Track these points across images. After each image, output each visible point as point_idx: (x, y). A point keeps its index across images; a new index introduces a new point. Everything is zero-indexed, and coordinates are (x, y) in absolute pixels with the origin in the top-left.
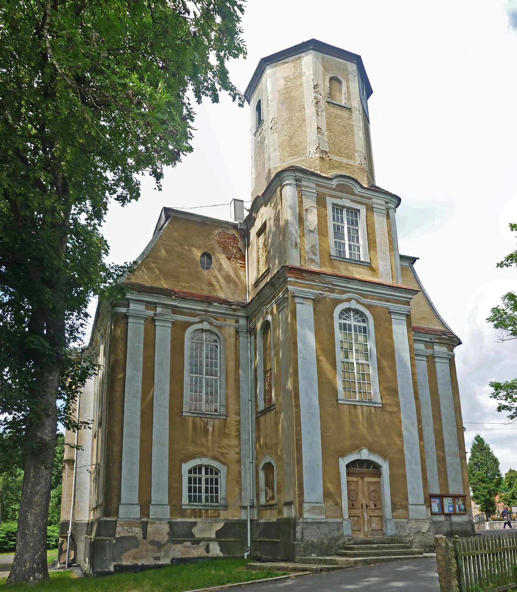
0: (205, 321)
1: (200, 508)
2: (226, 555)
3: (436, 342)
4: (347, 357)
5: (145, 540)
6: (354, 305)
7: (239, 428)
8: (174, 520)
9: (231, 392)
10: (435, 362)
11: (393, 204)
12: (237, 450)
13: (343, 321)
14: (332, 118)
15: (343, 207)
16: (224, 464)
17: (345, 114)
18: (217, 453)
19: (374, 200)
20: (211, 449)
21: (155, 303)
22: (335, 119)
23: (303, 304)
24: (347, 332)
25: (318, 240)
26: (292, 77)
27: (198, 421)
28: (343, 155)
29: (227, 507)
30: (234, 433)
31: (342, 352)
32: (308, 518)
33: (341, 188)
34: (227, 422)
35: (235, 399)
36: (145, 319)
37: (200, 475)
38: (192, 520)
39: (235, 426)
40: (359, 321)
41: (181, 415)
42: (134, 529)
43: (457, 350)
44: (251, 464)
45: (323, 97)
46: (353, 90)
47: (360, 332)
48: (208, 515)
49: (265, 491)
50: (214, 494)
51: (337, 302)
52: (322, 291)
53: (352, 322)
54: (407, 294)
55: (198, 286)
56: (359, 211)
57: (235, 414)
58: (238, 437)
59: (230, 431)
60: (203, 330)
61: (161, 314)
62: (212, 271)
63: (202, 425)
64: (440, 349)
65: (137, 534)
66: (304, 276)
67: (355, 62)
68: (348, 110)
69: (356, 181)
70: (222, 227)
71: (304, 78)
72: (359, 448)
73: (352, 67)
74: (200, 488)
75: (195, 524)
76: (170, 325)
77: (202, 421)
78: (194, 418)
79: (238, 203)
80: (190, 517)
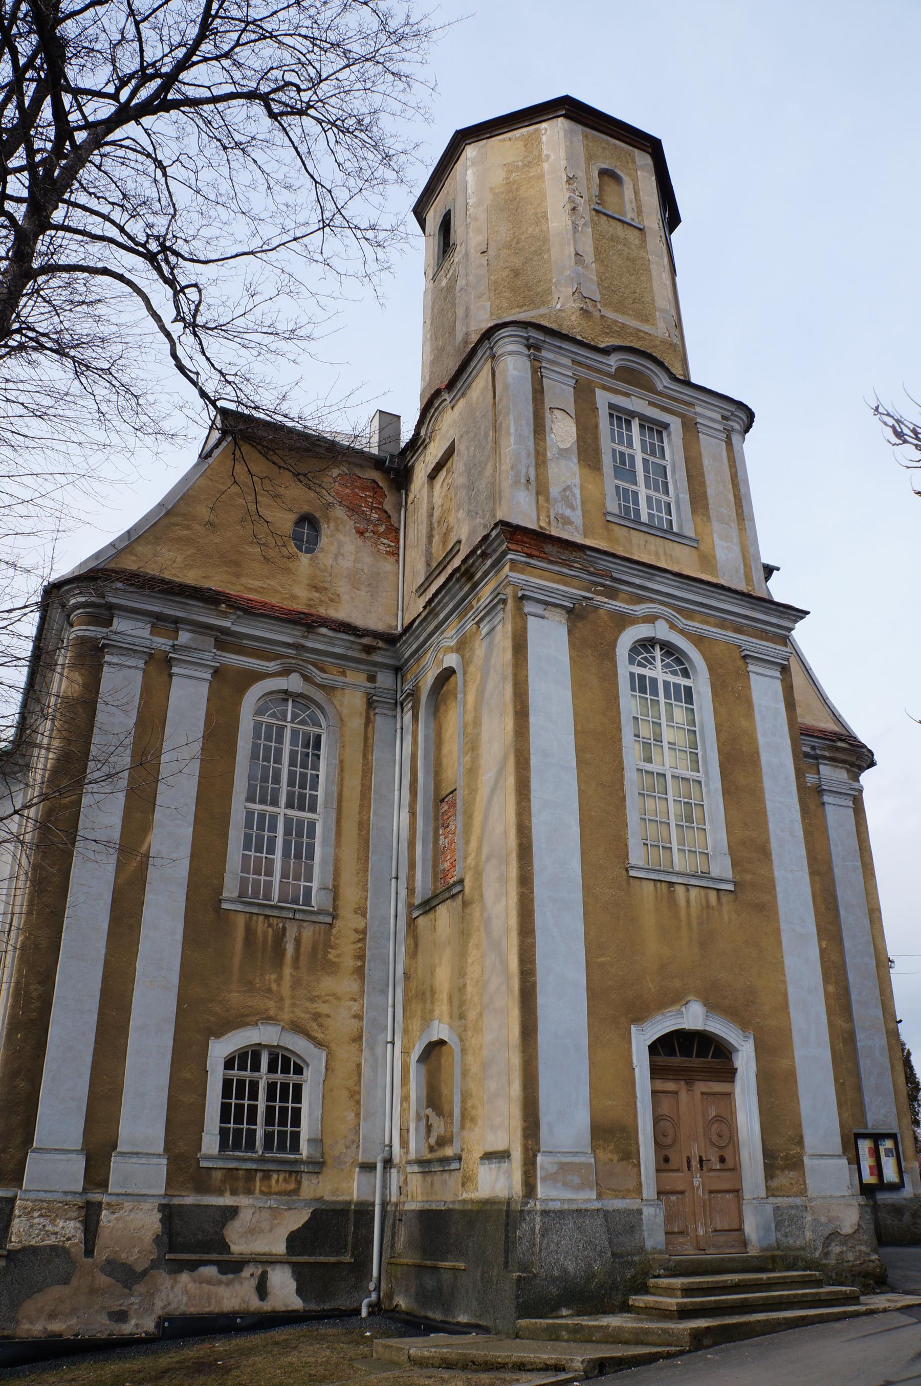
0: (294, 671)
1: (249, 1166)
2: (313, 1306)
3: (824, 757)
4: (649, 760)
5: (90, 1260)
6: (662, 631)
7: (363, 949)
8: (176, 1201)
9: (349, 853)
10: (823, 804)
11: (738, 423)
12: (355, 1007)
13: (638, 670)
14: (605, 241)
15: (633, 414)
16: (319, 1044)
17: (633, 235)
18: (302, 1015)
19: (698, 409)
20: (288, 1002)
21: (177, 621)
22: (611, 244)
23: (543, 617)
24: (648, 696)
25: (578, 476)
26: (520, 164)
27: (260, 925)
28: (631, 312)
29: (322, 1164)
30: (349, 962)
31: (636, 746)
32: (552, 1200)
33: (628, 376)
34: (334, 931)
35: (358, 873)
36: (146, 657)
37: (256, 1074)
38: (227, 1200)
39: (354, 943)
40: (674, 673)
41: (217, 909)
42: (61, 1223)
43: (867, 778)
44: (389, 1046)
45: (585, 201)
46: (646, 198)
47: (678, 699)
48: (270, 1186)
49: (424, 1122)
50: (289, 1129)
51: (623, 621)
52: (589, 591)
53: (658, 671)
54: (780, 617)
55: (285, 589)
56: (666, 426)
57: (356, 912)
58: (360, 972)
59: (339, 956)
60: (286, 695)
61: (186, 648)
62: (321, 555)
63: (270, 937)
64: (831, 774)
65: (69, 1239)
66: (546, 550)
67: (650, 150)
68: (637, 231)
69: (660, 364)
70: (349, 463)
71: (546, 166)
72: (680, 1000)
73: (644, 160)
74: (253, 1110)
75: (233, 1212)
76: (209, 676)
77: (270, 925)
78: (251, 919)
79: (389, 421)
80: (221, 1193)
